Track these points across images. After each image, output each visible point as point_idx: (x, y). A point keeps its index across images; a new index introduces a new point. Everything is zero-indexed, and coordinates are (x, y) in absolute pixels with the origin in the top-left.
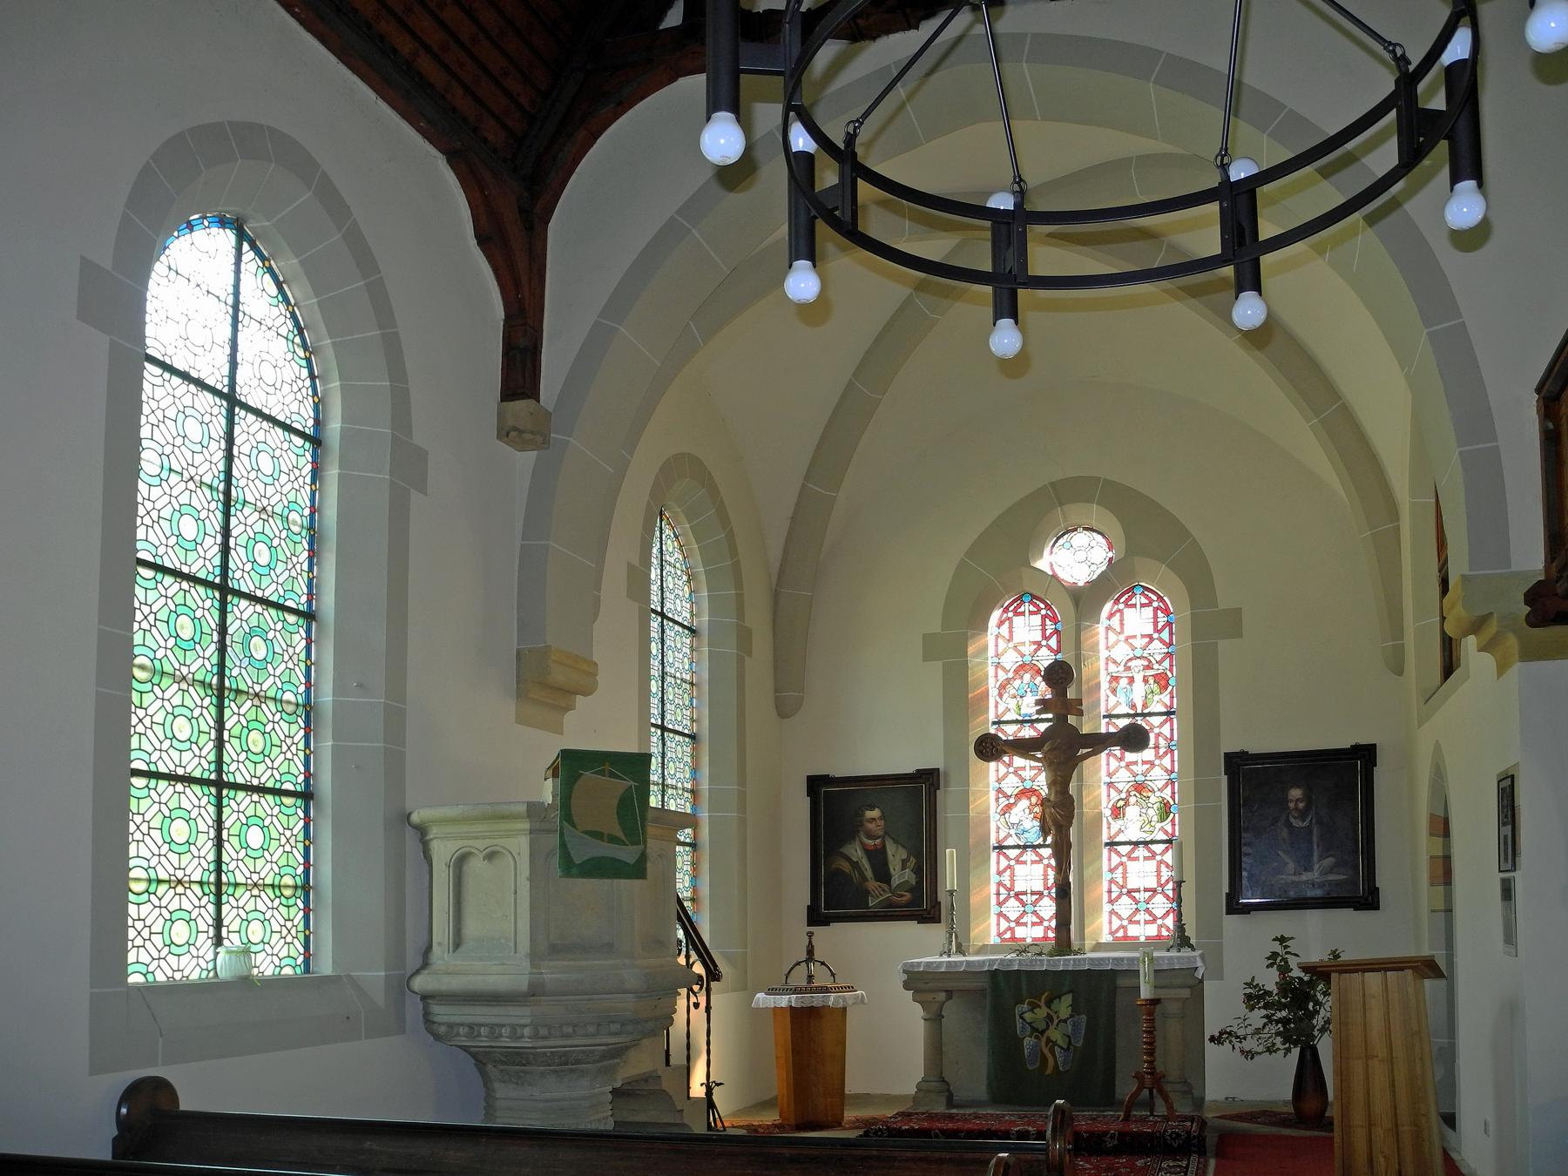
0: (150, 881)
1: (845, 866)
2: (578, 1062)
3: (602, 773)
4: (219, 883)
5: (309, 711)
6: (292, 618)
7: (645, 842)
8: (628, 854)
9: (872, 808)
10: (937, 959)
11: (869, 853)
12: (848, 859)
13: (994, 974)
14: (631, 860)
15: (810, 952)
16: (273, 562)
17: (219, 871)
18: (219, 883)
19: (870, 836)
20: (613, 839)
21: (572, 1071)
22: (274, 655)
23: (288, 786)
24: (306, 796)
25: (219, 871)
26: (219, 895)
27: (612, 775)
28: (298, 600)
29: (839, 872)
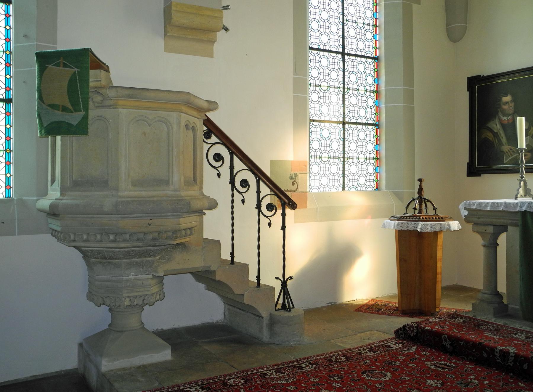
0: (329, 157)
1: (490, 136)
2: (111, 258)
3: (58, 65)
4: (344, 157)
5: (377, 92)
6: (370, 60)
7: (86, 109)
8: (74, 119)
9: (506, 95)
10: (512, 201)
11: (503, 125)
12: (491, 131)
13: (524, 214)
14: (75, 123)
15: (420, 191)
16: (362, 41)
17: (344, 153)
18: (344, 157)
19: (505, 115)
20: (65, 109)
21: (110, 263)
22: (362, 74)
23: (371, 122)
24: (377, 125)
25: (344, 153)
26: (344, 162)
27: (65, 65)
28: (371, 53)
29: (486, 140)
